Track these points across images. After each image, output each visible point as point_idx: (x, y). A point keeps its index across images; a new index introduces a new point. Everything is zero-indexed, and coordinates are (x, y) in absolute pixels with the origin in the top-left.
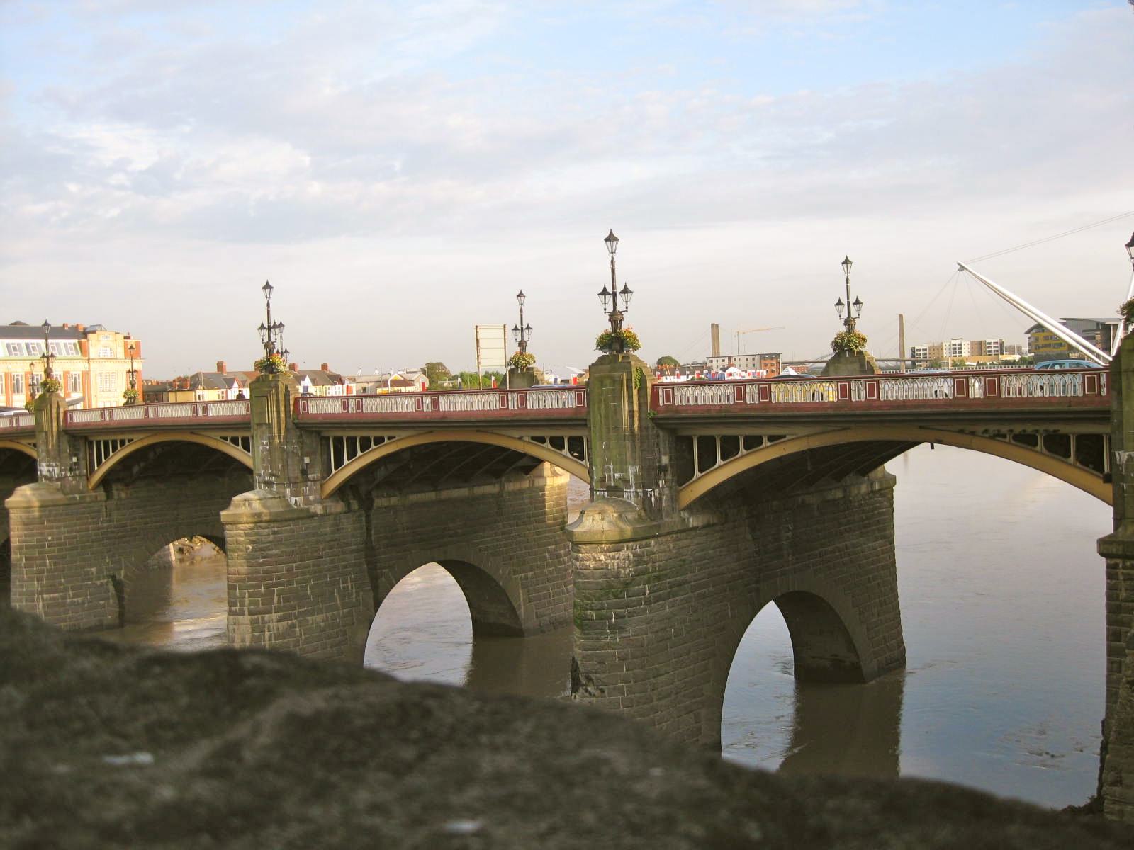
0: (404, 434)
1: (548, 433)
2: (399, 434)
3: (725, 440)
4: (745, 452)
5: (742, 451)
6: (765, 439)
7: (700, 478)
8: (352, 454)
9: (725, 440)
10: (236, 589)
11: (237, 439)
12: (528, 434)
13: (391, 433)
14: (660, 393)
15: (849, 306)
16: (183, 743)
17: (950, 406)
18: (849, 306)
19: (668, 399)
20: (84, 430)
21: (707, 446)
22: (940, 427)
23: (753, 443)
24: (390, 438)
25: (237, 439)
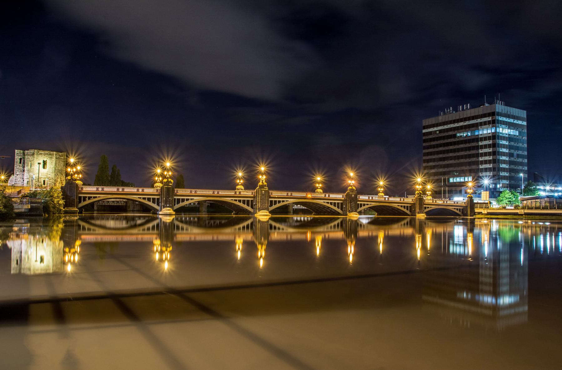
3: (364, 204)
5: (427, 209)
6: (93, 197)
24: (286, 201)
25: (402, 206)
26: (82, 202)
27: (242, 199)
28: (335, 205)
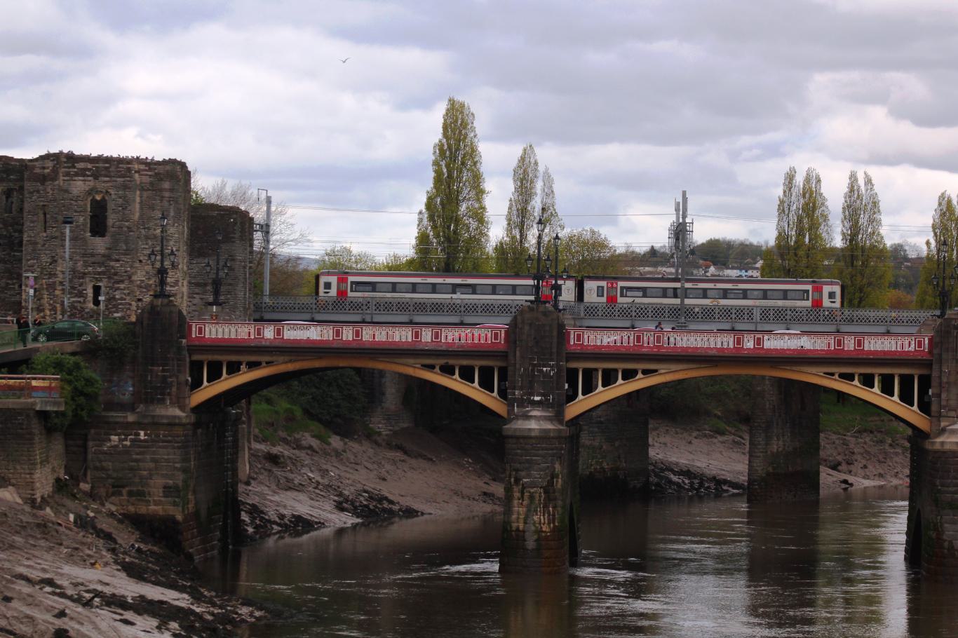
0: (674, 367)
2: (662, 367)
3: (210, 364)
4: (622, 382)
5: (620, 381)
6: (640, 372)
7: (581, 400)
8: (589, 389)
9: (210, 364)
10: (190, 461)
11: (471, 369)
12: (821, 370)
13: (268, 358)
14: (194, 329)
15: (946, 191)
16: (358, 517)
17: (476, 347)
18: (946, 191)
19: (200, 332)
20: (616, 354)
21: (196, 368)
22: (388, 360)
23: (629, 375)
24: (267, 363)
25: (471, 369)
26: (205, 383)
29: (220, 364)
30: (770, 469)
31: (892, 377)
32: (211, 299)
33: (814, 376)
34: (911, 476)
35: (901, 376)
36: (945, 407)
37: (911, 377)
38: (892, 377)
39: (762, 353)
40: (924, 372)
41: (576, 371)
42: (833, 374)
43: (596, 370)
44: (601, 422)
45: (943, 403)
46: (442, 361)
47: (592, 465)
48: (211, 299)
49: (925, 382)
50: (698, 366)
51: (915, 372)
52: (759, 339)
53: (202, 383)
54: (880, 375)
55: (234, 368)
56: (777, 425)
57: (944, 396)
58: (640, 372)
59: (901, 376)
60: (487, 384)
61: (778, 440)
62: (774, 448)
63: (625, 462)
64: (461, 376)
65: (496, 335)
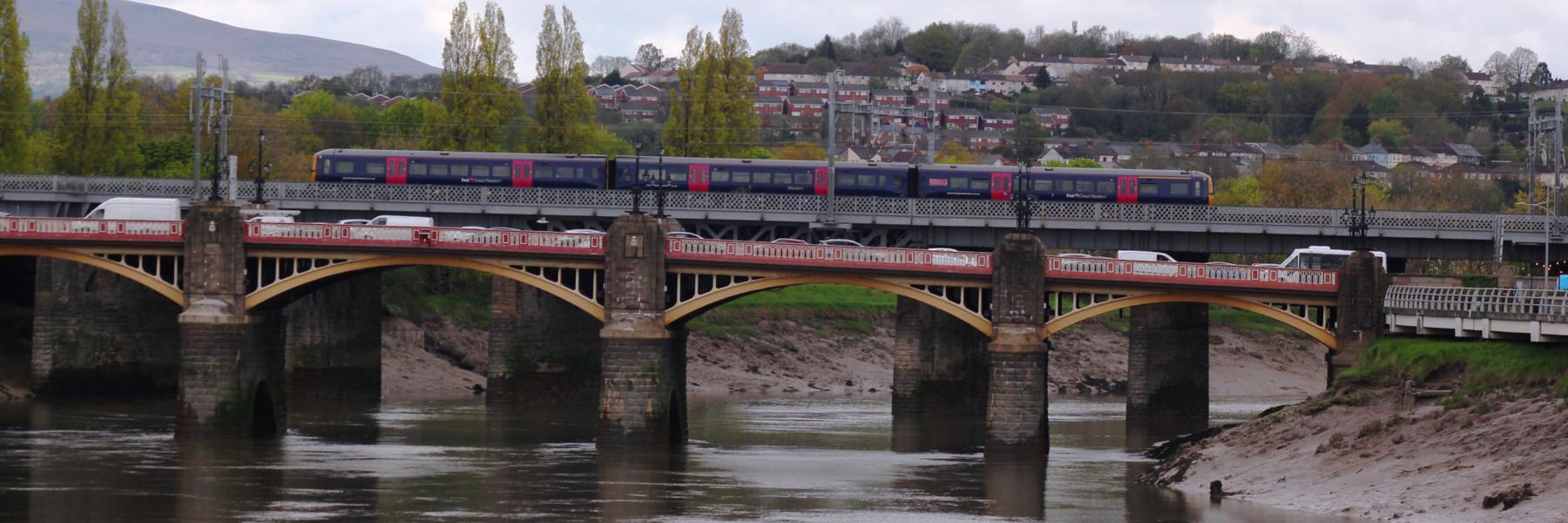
1: (542, 264)
2: (350, 257)
3: (300, 261)
6: (1110, 297)
11: (556, 270)
12: (506, 263)
24: (754, 278)
25: (556, 270)
27: (142, 252)
28: (150, 268)
29: (291, 261)
30: (300, 364)
31: (154, 258)
32: (656, 212)
33: (86, 258)
34: (685, 390)
35: (581, 271)
36: (193, 285)
37: (976, 290)
38: (154, 258)
39: (34, 237)
40: (986, 285)
41: (256, 260)
42: (102, 255)
43: (959, 289)
44: (115, 311)
45: (193, 281)
46: (931, 283)
47: (99, 359)
48: (656, 212)
49: (987, 294)
50: (1151, 293)
51: (980, 286)
52: (32, 224)
53: (694, 294)
54: (1328, 307)
55: (304, 266)
56: (312, 313)
57: (193, 275)
58: (1110, 297)
59: (581, 271)
60: (972, 305)
61: (313, 330)
62: (307, 340)
63: (151, 356)
64: (563, 282)
65: (174, 227)
